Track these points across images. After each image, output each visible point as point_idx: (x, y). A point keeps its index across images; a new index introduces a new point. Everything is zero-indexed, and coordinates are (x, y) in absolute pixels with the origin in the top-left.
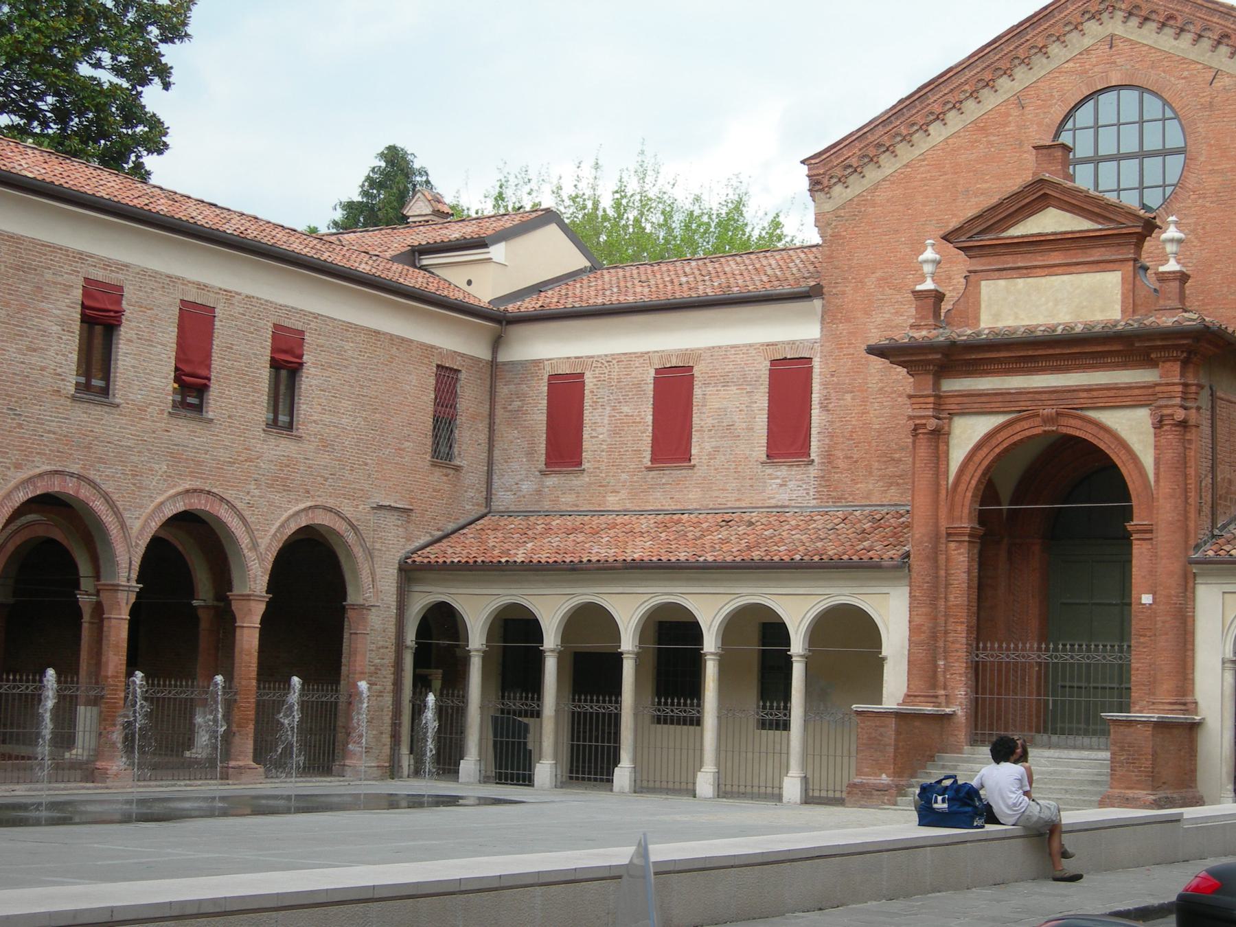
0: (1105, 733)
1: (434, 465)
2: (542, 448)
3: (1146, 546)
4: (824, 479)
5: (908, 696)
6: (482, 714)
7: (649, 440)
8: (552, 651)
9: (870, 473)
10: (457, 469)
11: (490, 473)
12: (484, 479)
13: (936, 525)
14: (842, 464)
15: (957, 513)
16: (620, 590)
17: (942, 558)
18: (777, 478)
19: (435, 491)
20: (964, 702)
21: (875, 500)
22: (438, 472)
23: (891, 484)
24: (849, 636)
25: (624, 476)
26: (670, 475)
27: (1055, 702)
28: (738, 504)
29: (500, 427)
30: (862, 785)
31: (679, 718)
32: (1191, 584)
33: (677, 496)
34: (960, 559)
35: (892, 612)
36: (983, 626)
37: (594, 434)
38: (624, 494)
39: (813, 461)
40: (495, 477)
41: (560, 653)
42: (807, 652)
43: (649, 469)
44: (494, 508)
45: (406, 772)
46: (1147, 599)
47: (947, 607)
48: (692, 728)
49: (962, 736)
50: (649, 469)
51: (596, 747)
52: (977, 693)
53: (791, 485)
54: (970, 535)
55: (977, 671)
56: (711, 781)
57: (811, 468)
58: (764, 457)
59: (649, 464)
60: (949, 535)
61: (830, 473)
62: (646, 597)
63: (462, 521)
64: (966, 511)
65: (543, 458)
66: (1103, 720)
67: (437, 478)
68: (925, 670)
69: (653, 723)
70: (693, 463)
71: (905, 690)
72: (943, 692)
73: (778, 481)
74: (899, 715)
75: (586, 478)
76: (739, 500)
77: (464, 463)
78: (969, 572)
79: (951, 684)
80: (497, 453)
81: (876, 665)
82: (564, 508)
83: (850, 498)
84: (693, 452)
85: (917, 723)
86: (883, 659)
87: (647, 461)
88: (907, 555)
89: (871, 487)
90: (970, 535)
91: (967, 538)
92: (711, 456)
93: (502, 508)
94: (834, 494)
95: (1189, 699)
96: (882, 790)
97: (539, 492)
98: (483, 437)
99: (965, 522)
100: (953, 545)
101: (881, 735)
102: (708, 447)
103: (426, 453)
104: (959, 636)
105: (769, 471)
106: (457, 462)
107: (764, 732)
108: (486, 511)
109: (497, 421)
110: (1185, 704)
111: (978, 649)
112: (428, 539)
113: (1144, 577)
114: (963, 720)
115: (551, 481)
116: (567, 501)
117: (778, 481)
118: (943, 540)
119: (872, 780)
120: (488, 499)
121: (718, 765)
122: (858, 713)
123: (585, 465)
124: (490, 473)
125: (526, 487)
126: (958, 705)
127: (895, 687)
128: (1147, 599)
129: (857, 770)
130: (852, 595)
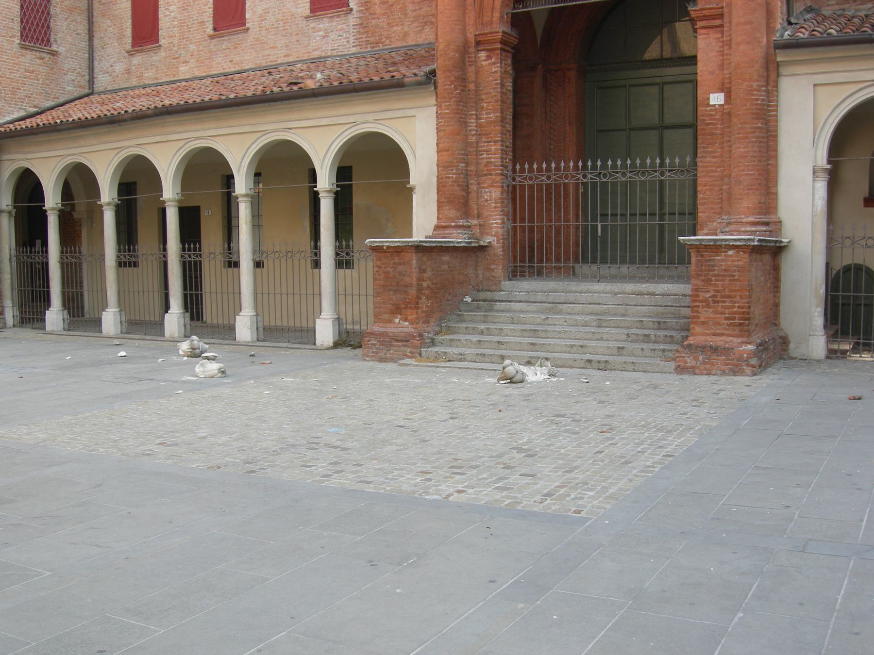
0: (684, 260)
1: (23, 47)
2: (128, 32)
3: (714, 35)
4: (363, 26)
5: (437, 228)
6: (549, 276)
7: (211, 11)
8: (109, 204)
9: (406, 15)
10: (54, 54)
11: (91, 59)
12: (85, 64)
13: (464, 31)
14: (378, 10)
15: (487, 19)
16: (158, 139)
17: (471, 70)
18: (319, 31)
19: (26, 71)
20: (500, 231)
21: (411, 42)
22: (29, 56)
23: (426, 23)
24: (373, 164)
25: (192, 47)
26: (226, 43)
27: (604, 228)
28: (287, 60)
29: (97, 19)
30: (382, 334)
31: (130, 263)
32: (773, 76)
33: (237, 59)
34: (492, 71)
35: (417, 132)
36: (522, 143)
37: (168, 13)
38: (192, 63)
39: (351, 10)
40: (96, 63)
41: (117, 206)
42: (335, 188)
43: (212, 37)
44: (96, 89)
45: (10, 320)
46: (717, 99)
47: (479, 126)
48: (130, 269)
49: (499, 271)
50: (212, 37)
51: (191, 289)
52: (514, 221)
53: (333, 36)
54: (502, 42)
55: (516, 198)
56: (249, 324)
57: (350, 17)
58: (308, 12)
59: (212, 32)
60: (478, 43)
61: (368, 19)
62: (182, 143)
63: (62, 100)
64: (497, 15)
65: (130, 40)
66: (682, 246)
67: (29, 59)
68: (457, 197)
69: (225, 267)
70: (247, 25)
71: (434, 221)
72: (475, 222)
73: (321, 33)
74: (420, 248)
75: (163, 54)
76: (287, 56)
77: (61, 50)
78: (502, 85)
79: (486, 213)
80: (96, 42)
81: (404, 193)
82: (147, 82)
83: (387, 42)
84: (247, 16)
85: (446, 258)
86: (411, 190)
87: (210, 30)
88: (433, 73)
89: (406, 29)
90: (502, 42)
91: (499, 46)
92: (262, 18)
93: (102, 89)
94: (372, 39)
95: (771, 218)
96: (405, 340)
97: (128, 71)
98: (82, 28)
99: (498, 26)
100: (483, 55)
101: (400, 273)
102: (259, 10)
103: (13, 36)
104: (493, 152)
105: (312, 25)
106: (54, 47)
107: (230, 270)
108: (87, 91)
109: (95, 14)
110: (767, 224)
111: (514, 170)
112: (22, 113)
113: (712, 73)
114: (500, 251)
115: (137, 59)
116: (149, 76)
117: (321, 33)
118: (472, 50)
119: (391, 329)
120: (91, 82)
121: (256, 308)
122: (376, 249)
123: (162, 42)
124: (91, 59)
125: (119, 68)
126: (494, 230)
127: (424, 220)
128: (717, 99)
129: (375, 316)
130: (376, 121)
